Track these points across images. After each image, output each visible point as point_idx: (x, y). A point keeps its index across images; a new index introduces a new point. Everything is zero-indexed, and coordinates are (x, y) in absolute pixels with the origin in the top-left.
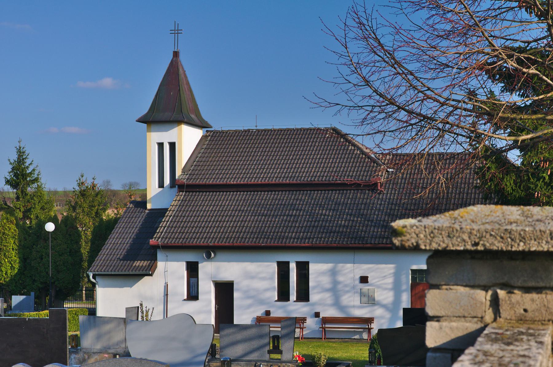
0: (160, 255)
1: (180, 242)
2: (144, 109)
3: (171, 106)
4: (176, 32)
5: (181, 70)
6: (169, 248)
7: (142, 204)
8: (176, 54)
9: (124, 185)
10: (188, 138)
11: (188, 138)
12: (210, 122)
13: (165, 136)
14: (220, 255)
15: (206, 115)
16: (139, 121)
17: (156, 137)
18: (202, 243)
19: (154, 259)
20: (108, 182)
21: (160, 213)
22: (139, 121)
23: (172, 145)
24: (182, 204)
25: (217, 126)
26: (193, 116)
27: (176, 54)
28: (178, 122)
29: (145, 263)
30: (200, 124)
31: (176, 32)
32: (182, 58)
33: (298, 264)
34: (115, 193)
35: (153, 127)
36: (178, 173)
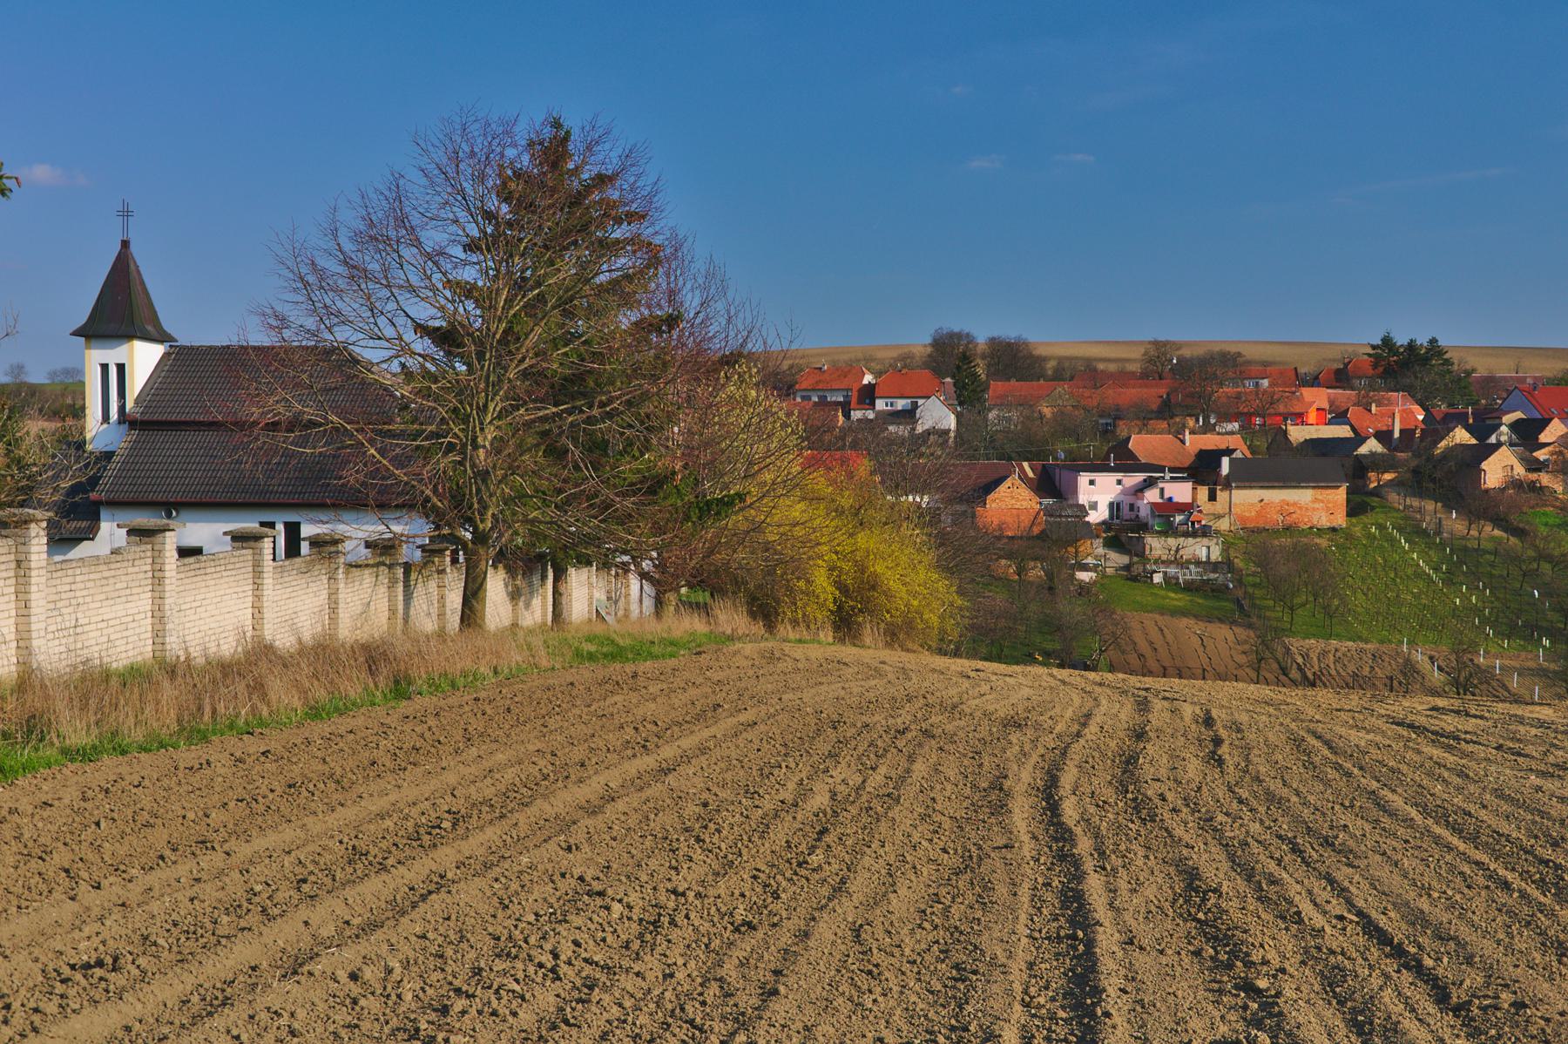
0: (104, 513)
1: (131, 497)
2: (82, 318)
3: (119, 312)
4: (126, 213)
5: (132, 266)
6: (115, 504)
7: (80, 445)
8: (125, 244)
9: (53, 374)
10: (144, 358)
11: (144, 358)
12: (175, 335)
13: (112, 355)
14: (185, 514)
15: (168, 326)
16: (75, 333)
17: (96, 357)
18: (160, 498)
19: (96, 519)
20: (20, 368)
21: (108, 456)
22: (75, 333)
23: (121, 368)
24: (134, 448)
25: (185, 338)
26: (149, 328)
27: (125, 244)
28: (130, 337)
29: (84, 524)
30: (160, 337)
31: (126, 213)
32: (134, 249)
33: (286, 524)
34: (33, 390)
35: (93, 342)
36: (129, 405)
